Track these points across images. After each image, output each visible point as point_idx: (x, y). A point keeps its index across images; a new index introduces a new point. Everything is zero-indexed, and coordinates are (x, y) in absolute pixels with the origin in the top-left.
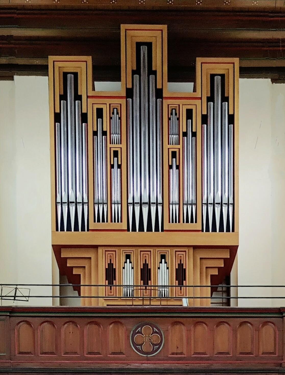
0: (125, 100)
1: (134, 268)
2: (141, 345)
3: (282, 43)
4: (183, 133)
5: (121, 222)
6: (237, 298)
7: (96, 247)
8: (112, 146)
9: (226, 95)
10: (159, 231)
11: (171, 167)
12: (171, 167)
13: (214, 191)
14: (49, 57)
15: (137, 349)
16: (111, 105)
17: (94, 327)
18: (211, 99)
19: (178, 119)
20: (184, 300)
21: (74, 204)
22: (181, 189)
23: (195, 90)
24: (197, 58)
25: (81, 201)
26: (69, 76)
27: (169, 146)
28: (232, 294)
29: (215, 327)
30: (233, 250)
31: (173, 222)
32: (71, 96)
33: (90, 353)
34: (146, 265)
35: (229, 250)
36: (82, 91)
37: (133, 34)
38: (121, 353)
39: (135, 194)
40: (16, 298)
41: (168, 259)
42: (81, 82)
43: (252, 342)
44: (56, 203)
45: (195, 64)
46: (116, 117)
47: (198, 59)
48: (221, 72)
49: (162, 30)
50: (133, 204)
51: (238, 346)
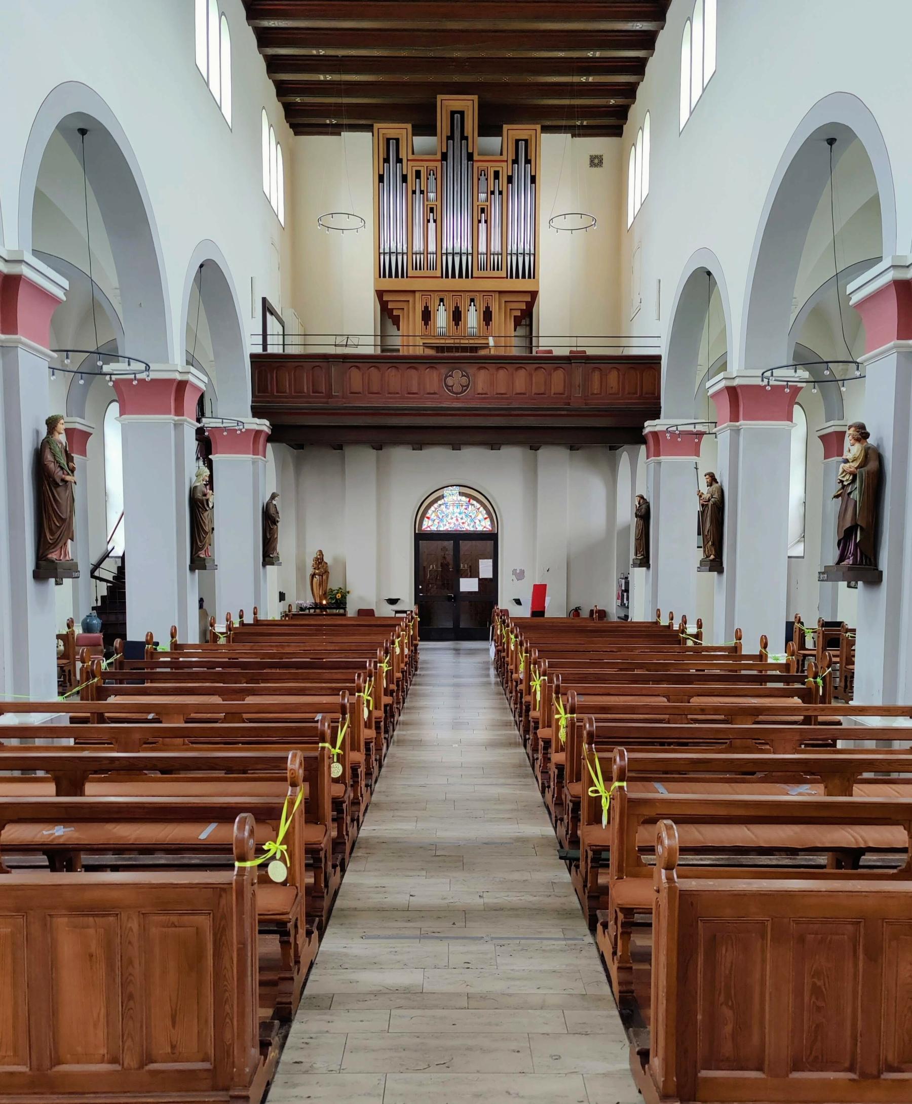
7: (414, 292)
11: (480, 221)
13: (518, 241)
15: (449, 390)
18: (516, 161)
20: (491, 339)
22: (490, 241)
30: (534, 294)
33: (409, 393)
34: (457, 308)
36: (403, 155)
37: (447, 103)
38: (435, 393)
39: (448, 245)
41: (477, 302)
44: (380, 253)
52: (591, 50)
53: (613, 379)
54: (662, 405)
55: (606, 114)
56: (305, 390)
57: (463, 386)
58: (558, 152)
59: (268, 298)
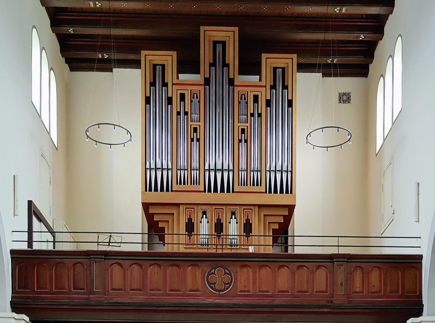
0: (203, 87)
1: (210, 222)
2: (214, 284)
3: (330, 50)
4: (251, 114)
5: (199, 184)
6: (294, 236)
7: (178, 205)
8: (192, 123)
9: (286, 84)
10: (230, 192)
11: (240, 141)
12: (240, 141)
13: (276, 160)
14: (142, 51)
16: (192, 91)
17: (175, 268)
18: (273, 87)
19: (247, 103)
21: (160, 170)
23: (260, 80)
24: (263, 54)
25: (166, 168)
26: (157, 67)
27: (239, 124)
28: (290, 243)
29: (277, 269)
30: (291, 208)
31: (241, 185)
32: (159, 84)
33: (172, 290)
34: (219, 220)
35: (287, 208)
36: (169, 79)
37: (210, 34)
38: (197, 290)
40: (111, 244)
41: (238, 216)
42: (168, 73)
43: (308, 282)
44: (146, 169)
45: (261, 60)
46: (195, 100)
47: (263, 55)
48: (282, 66)
49: (234, 32)
50: (209, 170)
51: (296, 285)
52: (338, 6)
53: (375, 277)
54: (425, 302)
55: (354, 56)
56: (67, 287)
57: (225, 284)
58: (312, 91)
59: (34, 201)
